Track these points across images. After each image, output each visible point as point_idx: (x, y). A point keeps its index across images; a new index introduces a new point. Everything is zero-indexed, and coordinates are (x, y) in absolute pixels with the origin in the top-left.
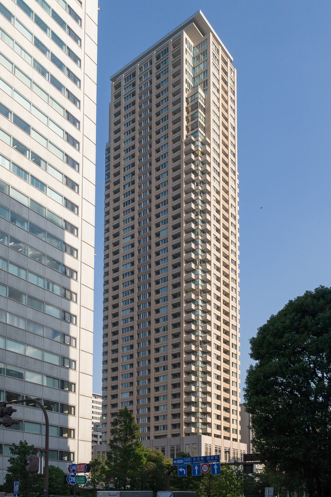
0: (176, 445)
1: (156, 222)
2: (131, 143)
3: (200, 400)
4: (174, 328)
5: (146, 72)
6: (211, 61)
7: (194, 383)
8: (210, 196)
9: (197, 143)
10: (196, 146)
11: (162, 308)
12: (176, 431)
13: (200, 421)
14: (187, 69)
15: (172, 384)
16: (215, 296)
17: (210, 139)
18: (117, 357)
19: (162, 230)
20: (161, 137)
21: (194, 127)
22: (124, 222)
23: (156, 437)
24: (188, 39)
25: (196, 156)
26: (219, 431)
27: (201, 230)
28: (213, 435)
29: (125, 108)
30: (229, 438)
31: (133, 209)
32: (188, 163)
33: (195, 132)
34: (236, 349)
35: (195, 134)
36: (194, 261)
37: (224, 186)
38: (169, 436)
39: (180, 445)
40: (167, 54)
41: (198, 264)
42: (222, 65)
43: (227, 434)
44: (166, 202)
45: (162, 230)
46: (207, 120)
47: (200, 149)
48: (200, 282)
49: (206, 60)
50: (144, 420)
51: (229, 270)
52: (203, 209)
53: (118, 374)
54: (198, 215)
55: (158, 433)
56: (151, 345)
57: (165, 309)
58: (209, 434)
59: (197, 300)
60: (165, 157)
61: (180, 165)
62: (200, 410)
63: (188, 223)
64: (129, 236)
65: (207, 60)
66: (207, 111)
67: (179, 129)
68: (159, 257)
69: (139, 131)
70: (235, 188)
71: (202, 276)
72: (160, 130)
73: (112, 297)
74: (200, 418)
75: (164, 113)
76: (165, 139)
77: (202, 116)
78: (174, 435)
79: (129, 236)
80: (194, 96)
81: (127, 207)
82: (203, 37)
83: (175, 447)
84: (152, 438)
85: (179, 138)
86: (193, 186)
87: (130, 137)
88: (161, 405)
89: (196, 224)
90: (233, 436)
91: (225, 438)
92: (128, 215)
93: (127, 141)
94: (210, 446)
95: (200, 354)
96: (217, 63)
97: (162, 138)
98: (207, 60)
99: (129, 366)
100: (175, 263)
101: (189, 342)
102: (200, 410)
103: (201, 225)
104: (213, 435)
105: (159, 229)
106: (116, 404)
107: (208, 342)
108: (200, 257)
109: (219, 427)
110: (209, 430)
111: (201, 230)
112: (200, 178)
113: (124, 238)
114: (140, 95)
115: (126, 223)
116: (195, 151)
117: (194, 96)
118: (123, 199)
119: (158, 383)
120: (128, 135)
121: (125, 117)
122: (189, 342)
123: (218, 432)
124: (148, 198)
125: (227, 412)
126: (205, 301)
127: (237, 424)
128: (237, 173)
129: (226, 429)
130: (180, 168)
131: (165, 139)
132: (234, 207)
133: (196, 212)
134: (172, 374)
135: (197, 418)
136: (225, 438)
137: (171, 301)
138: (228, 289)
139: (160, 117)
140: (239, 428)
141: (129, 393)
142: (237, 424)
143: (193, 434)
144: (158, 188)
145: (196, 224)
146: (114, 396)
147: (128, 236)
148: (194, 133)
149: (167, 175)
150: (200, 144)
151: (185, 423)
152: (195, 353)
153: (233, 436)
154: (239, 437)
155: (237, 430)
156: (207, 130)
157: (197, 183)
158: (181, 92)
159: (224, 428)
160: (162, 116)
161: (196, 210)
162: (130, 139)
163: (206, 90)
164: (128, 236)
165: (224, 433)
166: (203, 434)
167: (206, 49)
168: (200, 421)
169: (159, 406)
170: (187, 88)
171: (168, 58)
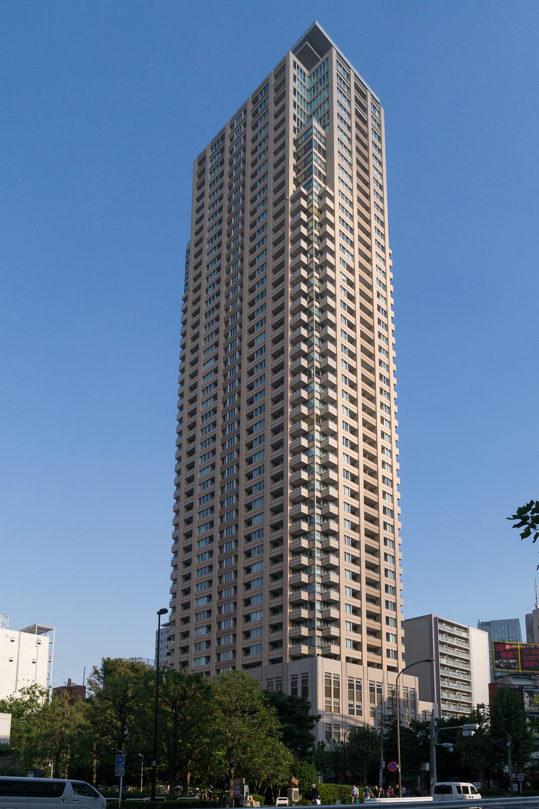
0: (276, 678)
1: (247, 503)
2: (211, 404)
3: (318, 545)
4: (273, 615)
5: (238, 140)
6: (335, 85)
7: (308, 468)
8: (335, 272)
9: (310, 197)
10: (309, 202)
11: (255, 518)
12: (276, 654)
13: (318, 633)
14: (296, 114)
15: (270, 626)
16: (348, 458)
17: (333, 190)
18: (188, 601)
19: (258, 336)
20: (254, 470)
21: (305, 174)
22: (203, 445)
23: (246, 667)
24: (298, 63)
25: (309, 215)
26: (359, 635)
27: (320, 465)
28: (343, 659)
29: (203, 417)
30: (379, 666)
31: (214, 424)
32: (296, 419)
33: (309, 155)
34: (393, 516)
35: (309, 186)
36: (307, 371)
37: (361, 223)
38: (265, 663)
39: (282, 677)
40: (264, 297)
41: (313, 375)
42: (355, 82)
43: (375, 658)
44: (262, 408)
45: (258, 336)
46: (329, 166)
47: (315, 204)
48: (317, 403)
49: (328, 86)
50: (228, 623)
51: (376, 434)
52: (323, 413)
53: (191, 569)
54: (313, 300)
55: (250, 659)
56: (244, 276)
57: (260, 581)
58: (336, 657)
59: (311, 433)
60: (261, 354)
61: (282, 489)
62: (318, 615)
63: (296, 391)
64: (209, 466)
65: (328, 85)
66: (327, 153)
67: (284, 184)
68: (251, 496)
69: (225, 306)
70: (384, 271)
71: (320, 394)
72: (252, 412)
73: (184, 562)
74: (319, 629)
75: (261, 261)
76: (259, 474)
77: (321, 160)
78: (273, 661)
79: (209, 466)
80: (306, 135)
81: (210, 318)
82: (318, 24)
83: (275, 680)
84: (239, 667)
85: (283, 197)
86: (304, 259)
87: (213, 330)
88: (252, 628)
89: (310, 314)
90: (388, 662)
91: (370, 664)
92: (206, 503)
93: (208, 349)
94: (337, 677)
95: (317, 520)
96: (346, 90)
97: (256, 471)
98: (328, 85)
99: (207, 555)
100: (274, 538)
101: (298, 501)
102: (318, 615)
103: (318, 316)
104: (343, 659)
105: (251, 452)
106: (188, 588)
107: (333, 568)
108: (317, 364)
109: (357, 646)
110: (334, 649)
111: (319, 324)
112: (315, 246)
113: (202, 470)
114: (226, 332)
115: (205, 446)
116: (307, 265)
117: (306, 135)
118: (204, 307)
119: (248, 641)
120: (205, 446)
121: (205, 339)
122: (298, 501)
123: (356, 654)
124: (239, 271)
125: (378, 638)
126: (326, 482)
127: (396, 642)
128: (388, 250)
129: (373, 649)
130: (282, 494)
131: (260, 442)
132: (391, 495)
133: (310, 297)
134: (270, 643)
135: (312, 629)
136: (370, 664)
137: (270, 487)
138: (374, 420)
139: (254, 378)
140: (402, 649)
141: (205, 628)
142: (396, 642)
143: (305, 656)
144: (250, 416)
145: (310, 314)
146: (186, 606)
147: (207, 467)
148: (306, 184)
149: (266, 254)
150: (315, 198)
151: (290, 638)
152: (308, 518)
153: (388, 662)
154: (402, 665)
155: (396, 653)
156: (328, 179)
157: (311, 255)
158: (285, 252)
159: (368, 648)
160: (256, 404)
161: (310, 294)
162: (212, 346)
163: (326, 123)
164: (207, 467)
165: (366, 656)
166: (324, 656)
167: (327, 71)
168: (318, 633)
169: (250, 614)
170: (296, 126)
171: (268, 97)
